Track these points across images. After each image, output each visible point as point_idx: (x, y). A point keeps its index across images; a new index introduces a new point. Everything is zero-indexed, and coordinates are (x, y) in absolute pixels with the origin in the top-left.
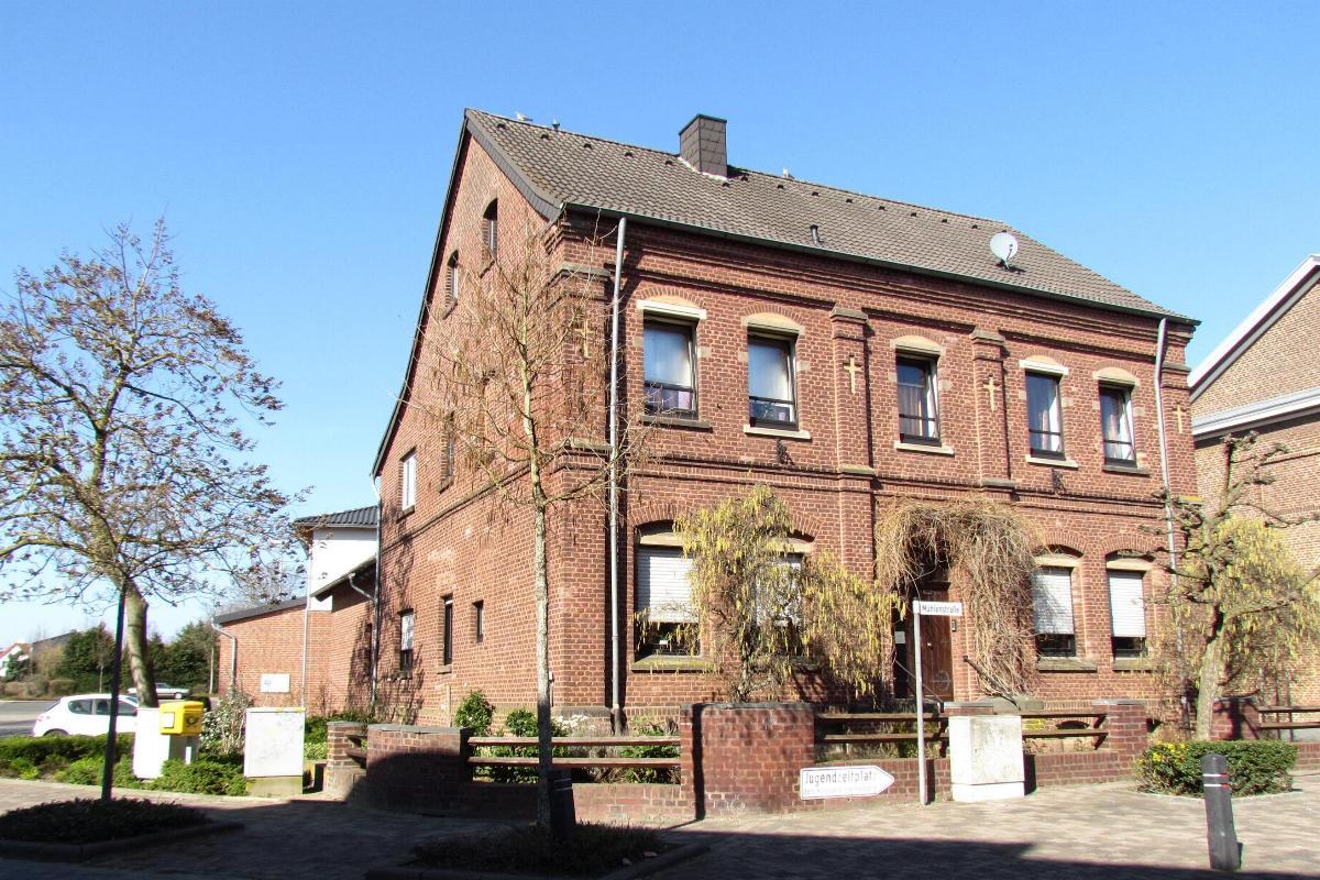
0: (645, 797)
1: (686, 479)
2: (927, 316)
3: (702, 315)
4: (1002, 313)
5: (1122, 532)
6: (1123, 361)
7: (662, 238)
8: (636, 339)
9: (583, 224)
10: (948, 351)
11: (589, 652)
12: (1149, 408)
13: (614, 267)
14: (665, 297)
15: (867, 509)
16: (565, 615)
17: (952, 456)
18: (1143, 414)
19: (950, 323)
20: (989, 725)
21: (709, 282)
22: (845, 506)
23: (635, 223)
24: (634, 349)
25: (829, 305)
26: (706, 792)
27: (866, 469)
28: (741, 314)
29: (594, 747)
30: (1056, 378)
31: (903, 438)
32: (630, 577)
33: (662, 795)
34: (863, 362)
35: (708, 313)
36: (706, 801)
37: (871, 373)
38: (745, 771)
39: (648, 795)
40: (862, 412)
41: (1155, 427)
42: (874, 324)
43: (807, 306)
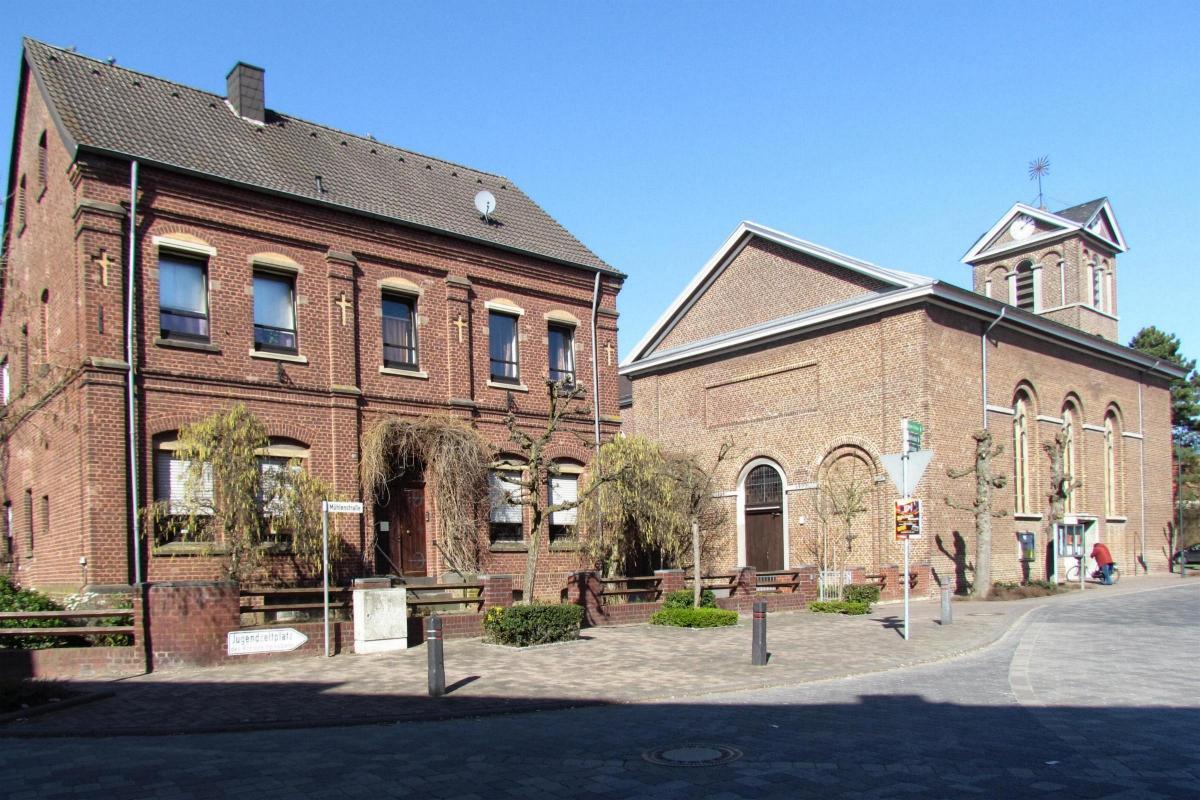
0: (109, 657)
1: (198, 395)
2: (407, 261)
3: (212, 251)
4: (471, 262)
5: (561, 443)
6: (568, 306)
7: (173, 181)
8: (151, 271)
9: (99, 164)
10: (426, 292)
11: (114, 540)
12: (587, 345)
13: (129, 204)
14: (179, 234)
15: (354, 422)
16: (91, 509)
17: (427, 379)
18: (582, 349)
19: (427, 268)
20: (379, 596)
21: (217, 223)
22: (336, 421)
23: (145, 167)
24: (149, 280)
25: (324, 248)
26: (154, 652)
27: (355, 389)
28: (247, 253)
29: (93, 618)
30: (515, 317)
31: (387, 364)
32: (150, 477)
33: (122, 655)
34: (352, 299)
35: (218, 251)
36: (154, 659)
37: (361, 308)
38: (183, 635)
39: (111, 655)
40: (351, 341)
41: (590, 359)
42: (363, 266)
43: (306, 248)
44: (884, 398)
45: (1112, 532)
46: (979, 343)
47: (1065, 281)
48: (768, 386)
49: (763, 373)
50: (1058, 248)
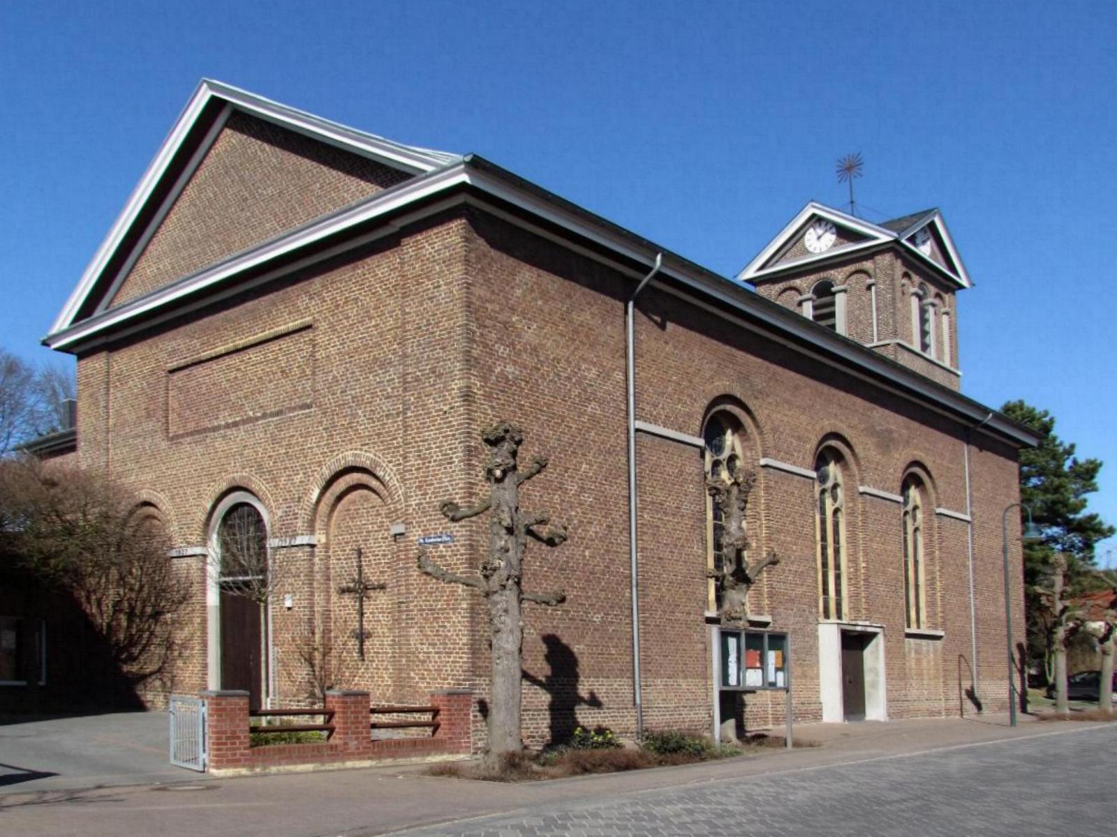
44: (405, 382)
45: (917, 652)
46: (621, 313)
47: (877, 309)
48: (247, 362)
49: (241, 343)
50: (867, 265)
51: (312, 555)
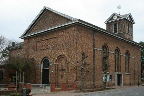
49: (47, 39)
51: (56, 66)
